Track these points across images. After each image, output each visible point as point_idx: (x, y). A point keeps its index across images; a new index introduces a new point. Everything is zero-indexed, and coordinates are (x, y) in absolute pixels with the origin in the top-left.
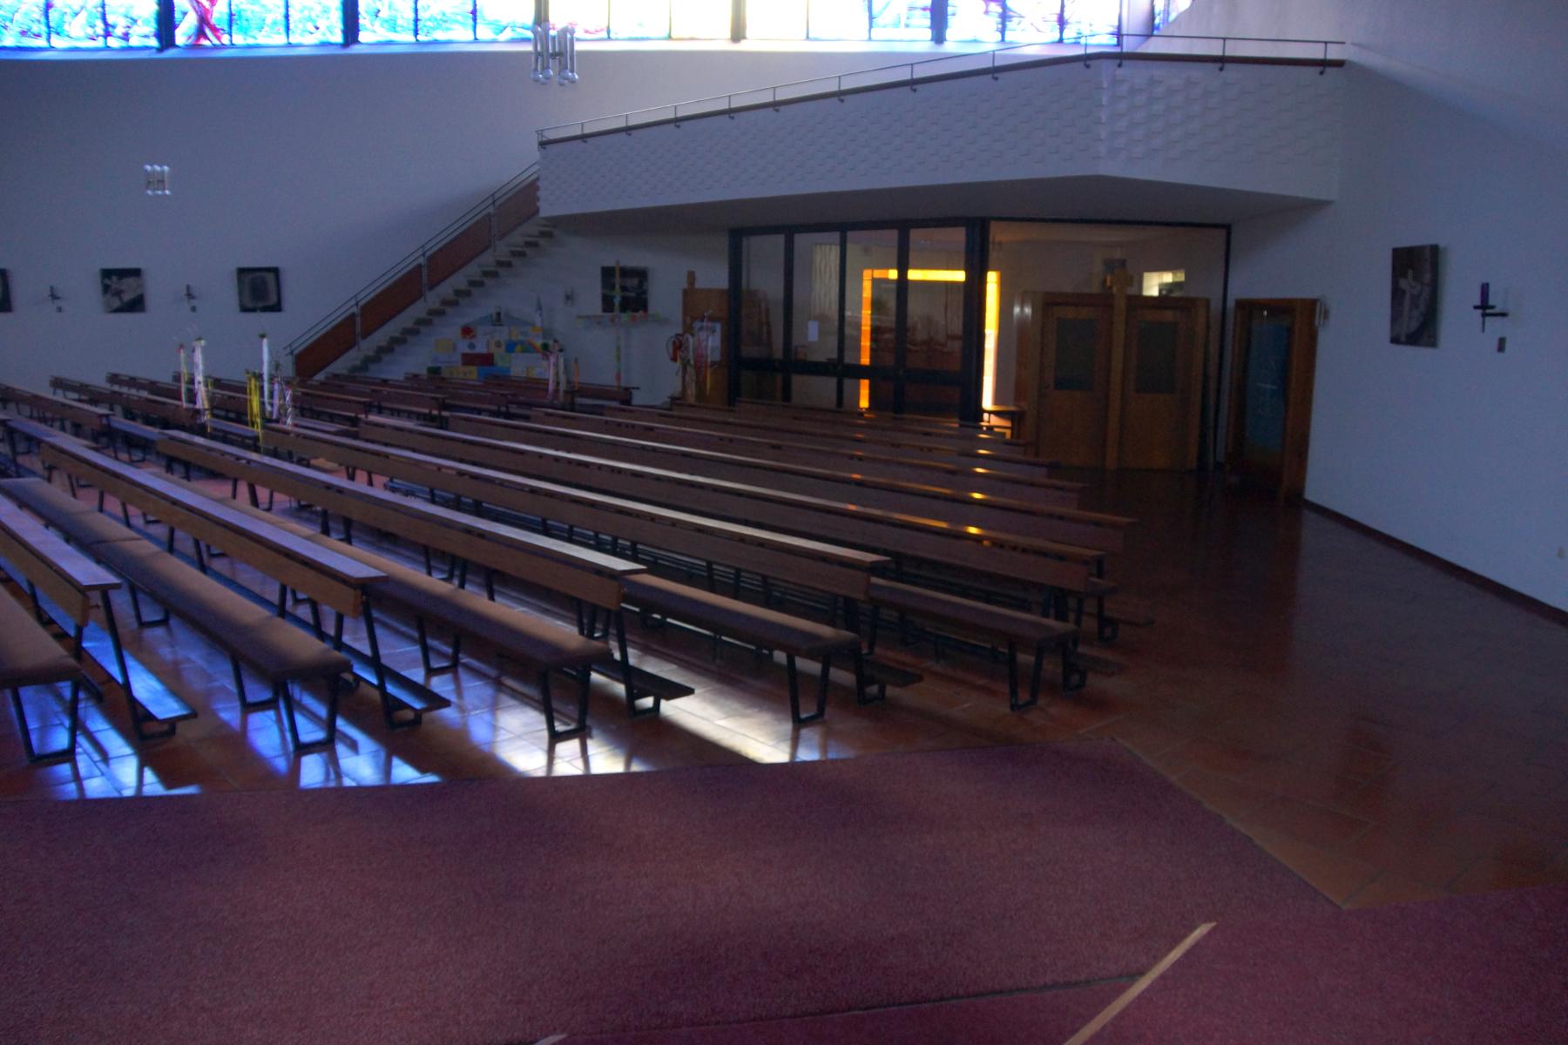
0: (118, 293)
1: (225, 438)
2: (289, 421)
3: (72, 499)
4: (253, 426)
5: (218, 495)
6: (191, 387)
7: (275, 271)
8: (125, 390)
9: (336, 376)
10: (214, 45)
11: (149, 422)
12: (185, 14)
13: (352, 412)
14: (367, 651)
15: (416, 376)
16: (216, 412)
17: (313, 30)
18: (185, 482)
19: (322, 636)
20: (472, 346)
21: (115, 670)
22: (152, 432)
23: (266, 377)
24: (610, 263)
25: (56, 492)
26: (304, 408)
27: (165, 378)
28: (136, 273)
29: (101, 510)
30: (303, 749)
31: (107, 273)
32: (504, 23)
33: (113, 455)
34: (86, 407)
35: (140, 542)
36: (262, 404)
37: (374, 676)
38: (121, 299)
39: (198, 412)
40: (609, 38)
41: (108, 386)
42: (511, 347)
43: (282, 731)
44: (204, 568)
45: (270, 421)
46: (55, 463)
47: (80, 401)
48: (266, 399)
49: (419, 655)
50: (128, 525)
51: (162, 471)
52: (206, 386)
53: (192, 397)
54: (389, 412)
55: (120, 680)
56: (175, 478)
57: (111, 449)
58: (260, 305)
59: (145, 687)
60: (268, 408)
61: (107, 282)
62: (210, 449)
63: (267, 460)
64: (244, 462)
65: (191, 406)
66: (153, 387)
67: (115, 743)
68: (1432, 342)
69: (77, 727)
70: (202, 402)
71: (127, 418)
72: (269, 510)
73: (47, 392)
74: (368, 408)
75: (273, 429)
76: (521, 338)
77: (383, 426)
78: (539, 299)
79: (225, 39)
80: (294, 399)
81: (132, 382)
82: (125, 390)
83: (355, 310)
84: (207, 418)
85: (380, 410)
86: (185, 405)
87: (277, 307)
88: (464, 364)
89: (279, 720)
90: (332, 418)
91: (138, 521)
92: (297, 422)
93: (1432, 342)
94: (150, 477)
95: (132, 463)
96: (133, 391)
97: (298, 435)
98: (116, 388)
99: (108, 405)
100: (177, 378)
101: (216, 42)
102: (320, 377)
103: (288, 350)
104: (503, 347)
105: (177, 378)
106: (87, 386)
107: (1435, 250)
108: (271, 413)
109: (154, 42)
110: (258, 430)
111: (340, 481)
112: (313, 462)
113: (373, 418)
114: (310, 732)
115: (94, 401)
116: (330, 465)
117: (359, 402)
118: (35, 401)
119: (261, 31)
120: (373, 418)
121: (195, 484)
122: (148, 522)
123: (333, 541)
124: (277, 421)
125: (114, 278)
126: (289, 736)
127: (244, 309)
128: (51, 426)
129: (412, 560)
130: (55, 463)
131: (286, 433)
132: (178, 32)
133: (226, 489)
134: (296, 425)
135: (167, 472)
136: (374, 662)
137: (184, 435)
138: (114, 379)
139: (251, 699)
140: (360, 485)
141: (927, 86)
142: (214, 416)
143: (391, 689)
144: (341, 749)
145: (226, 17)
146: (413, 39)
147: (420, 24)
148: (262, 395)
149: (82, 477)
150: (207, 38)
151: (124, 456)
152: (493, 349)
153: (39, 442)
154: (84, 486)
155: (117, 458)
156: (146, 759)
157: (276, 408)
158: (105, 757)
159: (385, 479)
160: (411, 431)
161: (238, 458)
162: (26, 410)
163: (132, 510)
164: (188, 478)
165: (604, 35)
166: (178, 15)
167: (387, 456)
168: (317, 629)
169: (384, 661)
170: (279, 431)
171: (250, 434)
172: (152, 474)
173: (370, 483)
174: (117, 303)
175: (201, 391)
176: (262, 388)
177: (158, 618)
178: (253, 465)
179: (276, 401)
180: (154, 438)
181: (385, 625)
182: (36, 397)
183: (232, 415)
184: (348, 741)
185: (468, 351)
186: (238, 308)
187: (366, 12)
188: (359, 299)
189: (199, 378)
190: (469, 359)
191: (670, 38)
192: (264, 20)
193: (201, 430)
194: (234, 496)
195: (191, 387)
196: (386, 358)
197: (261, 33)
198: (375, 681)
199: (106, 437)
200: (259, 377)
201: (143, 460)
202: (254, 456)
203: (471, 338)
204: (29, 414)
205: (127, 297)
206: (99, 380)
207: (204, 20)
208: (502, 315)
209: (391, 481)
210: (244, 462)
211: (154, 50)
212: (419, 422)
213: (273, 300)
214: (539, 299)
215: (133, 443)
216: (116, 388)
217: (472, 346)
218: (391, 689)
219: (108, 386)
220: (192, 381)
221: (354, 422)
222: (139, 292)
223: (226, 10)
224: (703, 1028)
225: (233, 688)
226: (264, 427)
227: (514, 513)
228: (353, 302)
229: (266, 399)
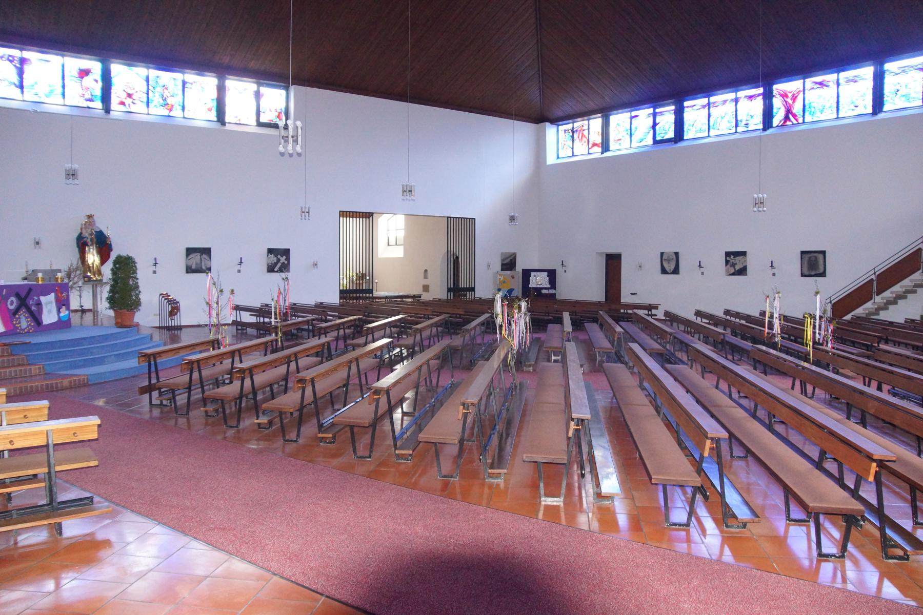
0: (733, 265)
1: (787, 351)
2: (829, 345)
3: (702, 379)
4: (807, 346)
5: (784, 387)
6: (770, 320)
7: (823, 253)
8: (733, 319)
9: (858, 318)
11: (744, 338)
13: (869, 342)
14: (874, 501)
15: (913, 321)
16: (783, 335)
17: (854, 108)
18: (763, 375)
19: (844, 487)
21: (717, 483)
22: (747, 345)
23: (818, 318)
25: (692, 373)
26: (840, 336)
27: (756, 314)
28: (744, 254)
29: (717, 387)
30: (822, 556)
31: (728, 254)
33: (725, 356)
34: (712, 327)
35: (737, 409)
36: (814, 333)
37: (878, 521)
39: (774, 335)
41: (724, 316)
43: (809, 540)
44: (770, 428)
45: (819, 344)
46: (697, 357)
47: (709, 324)
48: (817, 331)
49: (910, 511)
50: (730, 397)
51: (751, 368)
52: (780, 320)
53: (771, 326)
54: (904, 345)
55: (719, 489)
56: (757, 372)
57: (724, 352)
59: (732, 498)
60: (817, 336)
61: (728, 258)
62: (778, 358)
63: (814, 368)
64: (801, 368)
65: (770, 331)
66: (748, 318)
67: (710, 524)
69: (692, 513)
70: (777, 329)
71: (733, 335)
72: (811, 398)
73: (692, 317)
74: (880, 339)
75: (819, 349)
77: (889, 352)
78: (22, 92)
80: (834, 331)
81: (737, 315)
82: (733, 319)
83: (873, 277)
84: (778, 339)
85: (887, 342)
86: (767, 330)
87: (823, 274)
89: (808, 534)
90: (853, 344)
91: (735, 395)
92: (835, 346)
94: (744, 370)
95: (733, 361)
96: (737, 320)
97: (834, 354)
98: (728, 317)
99: (723, 327)
100: (763, 314)
102: (848, 317)
103: (828, 301)
105: (763, 314)
106: (714, 316)
108: (819, 339)
110: (810, 349)
111: (859, 385)
112: (841, 371)
113: (883, 346)
114: (829, 548)
115: (716, 325)
116: (851, 374)
117: (875, 336)
118: (686, 322)
120: (882, 346)
121: (769, 378)
122: (740, 397)
123: (852, 423)
124: (822, 344)
126: (814, 546)
127: (803, 275)
128: (693, 337)
129: (907, 444)
130: (697, 357)
131: (827, 352)
133: (788, 382)
134: (833, 348)
135: (754, 369)
136: (879, 511)
137: (764, 348)
138: (727, 312)
139: (793, 516)
140: (872, 390)
142: (782, 338)
143: (889, 532)
144: (848, 564)
148: (814, 327)
149: (708, 367)
150: (790, 120)
151: (730, 357)
153: (687, 345)
154: (707, 372)
155: (726, 358)
156: (727, 539)
157: (822, 336)
158: (703, 531)
159: (889, 387)
160: (908, 357)
161: (798, 365)
162: (682, 327)
163: (733, 389)
164: (765, 373)
166: (775, 110)
167: (892, 372)
168: (840, 482)
169: (886, 512)
170: (823, 350)
171: (804, 351)
172: (746, 369)
173: (879, 388)
174: (732, 271)
175: (776, 322)
176: (814, 323)
177: (742, 455)
178: (806, 370)
179: (823, 333)
180: (749, 349)
181: (888, 487)
182: (687, 320)
183: (792, 338)
184: (853, 559)
186: (800, 275)
188: (876, 271)
189: (776, 315)
193: (774, 346)
194: (793, 388)
195: (770, 320)
196: (891, 307)
198: (878, 524)
199: (720, 345)
200: (814, 318)
201: (740, 360)
202: (806, 365)
204: (683, 329)
205: (737, 268)
206: (720, 313)
207: (789, 111)
209: (893, 388)
210: (801, 368)
211: (761, 131)
212: (914, 351)
213: (821, 270)
214: (22, 92)
215: (735, 351)
216: (728, 317)
218: (889, 532)
219: (724, 316)
220: (771, 317)
221: (868, 347)
222: (744, 265)
224: (489, 353)
225: (783, 507)
226: (813, 348)
228: (872, 272)
229: (817, 331)
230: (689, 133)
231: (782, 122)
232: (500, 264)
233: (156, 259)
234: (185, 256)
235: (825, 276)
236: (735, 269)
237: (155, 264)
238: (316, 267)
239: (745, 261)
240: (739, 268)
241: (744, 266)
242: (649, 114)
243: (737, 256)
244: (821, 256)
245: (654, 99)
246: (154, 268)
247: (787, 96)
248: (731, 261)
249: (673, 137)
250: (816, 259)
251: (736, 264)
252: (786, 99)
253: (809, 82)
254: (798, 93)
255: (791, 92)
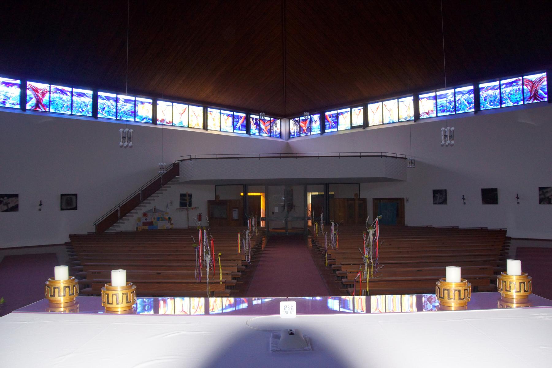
10: (42, 111)
12: (31, 98)
20: (146, 219)
24: (184, 192)
28: (16, 196)
32: (144, 116)
38: (8, 206)
40: (172, 125)
42: (158, 219)
58: (69, 208)
68: (446, 203)
76: (162, 216)
79: (47, 110)
83: (118, 208)
87: (75, 208)
88: (143, 225)
93: (446, 203)
101: (43, 110)
104: (156, 219)
107: (446, 190)
109: (18, 107)
119: (62, 109)
125: (6, 198)
132: (28, 105)
141: (363, 157)
145: (48, 102)
146: (70, 113)
147: (118, 114)
152: (153, 220)
165: (171, 124)
166: (28, 99)
185: (145, 221)
187: (100, 108)
190: (145, 224)
191: (188, 127)
192: (64, 105)
197: (62, 110)
203: (146, 217)
208: (156, 209)
213: (74, 206)
217: (146, 219)
222: (17, 203)
223: (48, 99)
227: (409, 240)
230: (371, 123)
231: (34, 108)
232: (538, 194)
233: (41, 201)
234: (538, 191)
235: (77, 209)
236: (8, 206)
237: (41, 204)
238: (407, 199)
239: (18, 201)
240: (11, 206)
241: (16, 205)
242: (421, 116)
243: (10, 198)
244: (74, 197)
245: (352, 104)
246: (39, 207)
247: (38, 92)
248: (5, 201)
249: (363, 124)
250: (71, 199)
251: (9, 203)
252: (37, 93)
253: (53, 87)
254: (47, 92)
255: (41, 90)
